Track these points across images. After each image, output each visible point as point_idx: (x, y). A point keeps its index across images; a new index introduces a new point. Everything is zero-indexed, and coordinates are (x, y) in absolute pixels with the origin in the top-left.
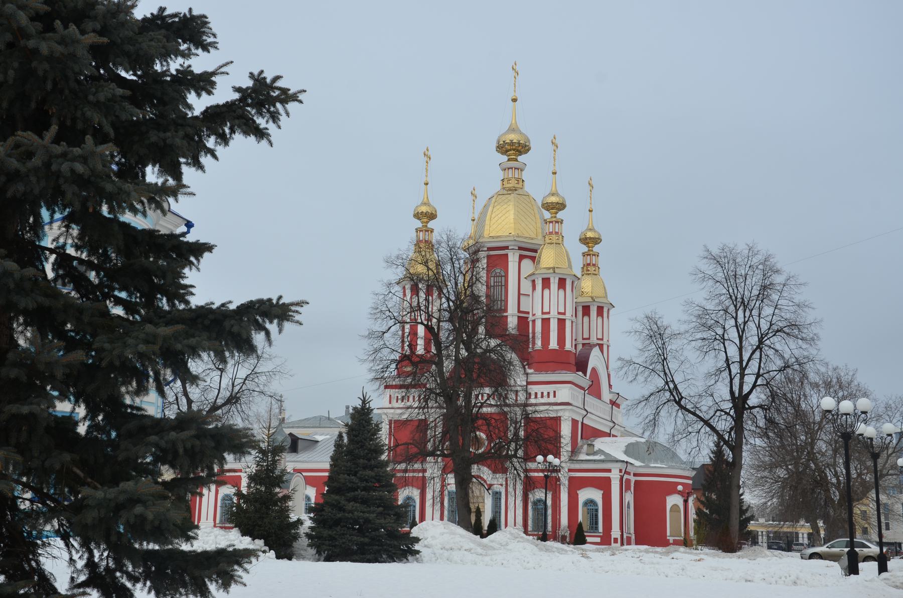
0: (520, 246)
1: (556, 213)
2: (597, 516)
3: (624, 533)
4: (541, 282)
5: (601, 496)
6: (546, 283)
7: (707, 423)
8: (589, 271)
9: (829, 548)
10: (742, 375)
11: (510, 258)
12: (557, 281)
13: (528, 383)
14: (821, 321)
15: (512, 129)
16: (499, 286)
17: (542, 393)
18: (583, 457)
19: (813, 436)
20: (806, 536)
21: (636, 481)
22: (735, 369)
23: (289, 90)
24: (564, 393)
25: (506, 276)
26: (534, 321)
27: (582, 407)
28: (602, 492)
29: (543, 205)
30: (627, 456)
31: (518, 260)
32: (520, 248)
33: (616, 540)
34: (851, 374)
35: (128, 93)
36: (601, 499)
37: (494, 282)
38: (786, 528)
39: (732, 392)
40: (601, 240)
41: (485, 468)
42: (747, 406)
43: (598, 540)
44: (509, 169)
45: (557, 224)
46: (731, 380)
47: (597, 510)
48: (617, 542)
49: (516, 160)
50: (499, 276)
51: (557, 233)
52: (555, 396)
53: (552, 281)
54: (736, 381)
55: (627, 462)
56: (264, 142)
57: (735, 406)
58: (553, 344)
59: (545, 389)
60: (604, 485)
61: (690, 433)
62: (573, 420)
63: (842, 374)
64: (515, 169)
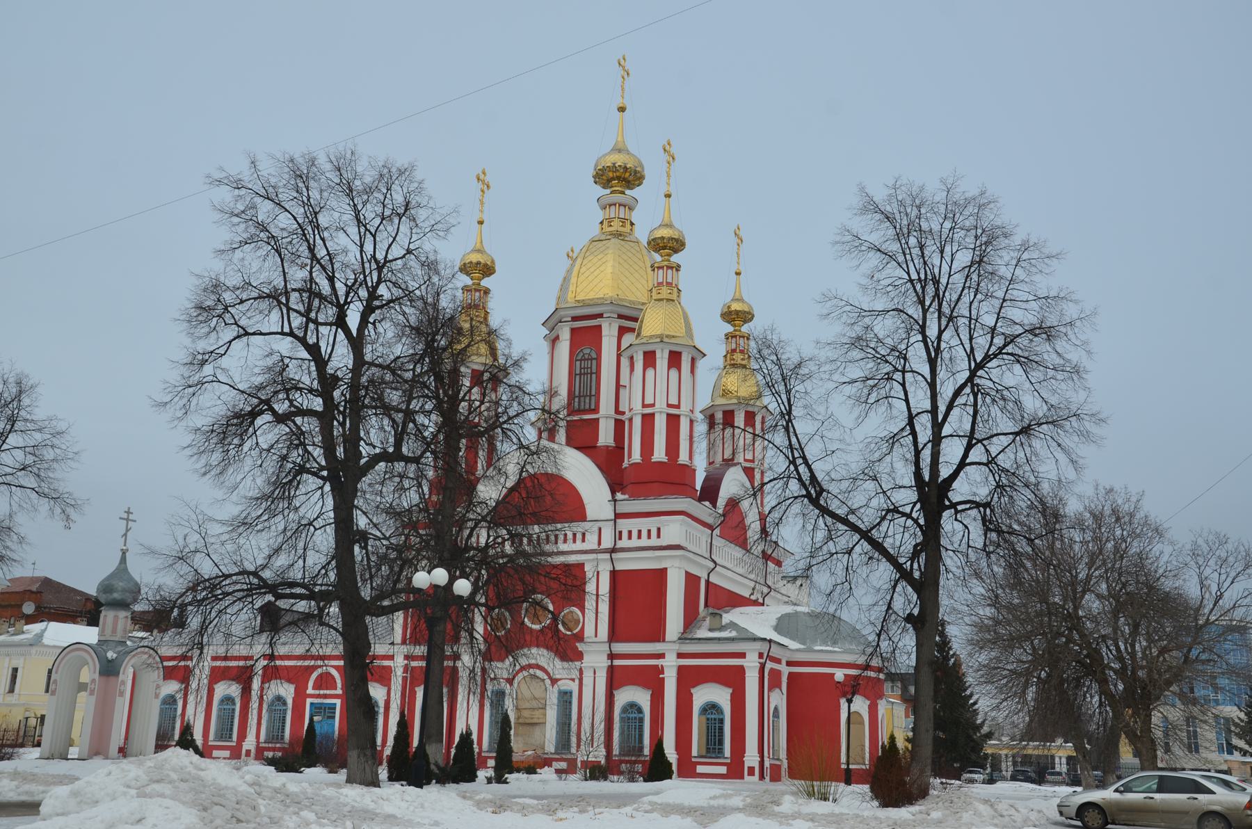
0: (620, 313)
1: (670, 255)
2: (721, 729)
3: (766, 759)
4: (642, 357)
5: (729, 698)
6: (650, 359)
7: (865, 535)
8: (734, 359)
9: (1121, 792)
10: (937, 439)
11: (605, 331)
12: (666, 355)
13: (618, 516)
14: (1094, 313)
15: (618, 150)
16: (584, 368)
17: (640, 532)
18: (703, 633)
19: (1076, 591)
20: (1064, 761)
21: (790, 674)
22: (925, 434)
24: (674, 531)
25: (599, 359)
26: (631, 420)
27: (707, 555)
28: (730, 691)
29: (649, 243)
30: (779, 633)
31: (616, 334)
32: (620, 317)
33: (751, 771)
34: (1134, 499)
36: (649, 703)
37: (581, 368)
38: (1033, 748)
39: (918, 474)
40: (753, 316)
41: (534, 650)
42: (947, 503)
43: (723, 770)
44: (610, 205)
45: (670, 271)
46: (917, 453)
47: (722, 721)
48: (754, 775)
49: (623, 193)
50: (588, 359)
51: (669, 284)
52: (659, 536)
53: (658, 355)
54: (926, 455)
55: (770, 641)
57: (923, 499)
58: (659, 454)
59: (644, 524)
60: (733, 678)
61: (832, 555)
62: (688, 574)
63: (1120, 502)
64: (620, 205)
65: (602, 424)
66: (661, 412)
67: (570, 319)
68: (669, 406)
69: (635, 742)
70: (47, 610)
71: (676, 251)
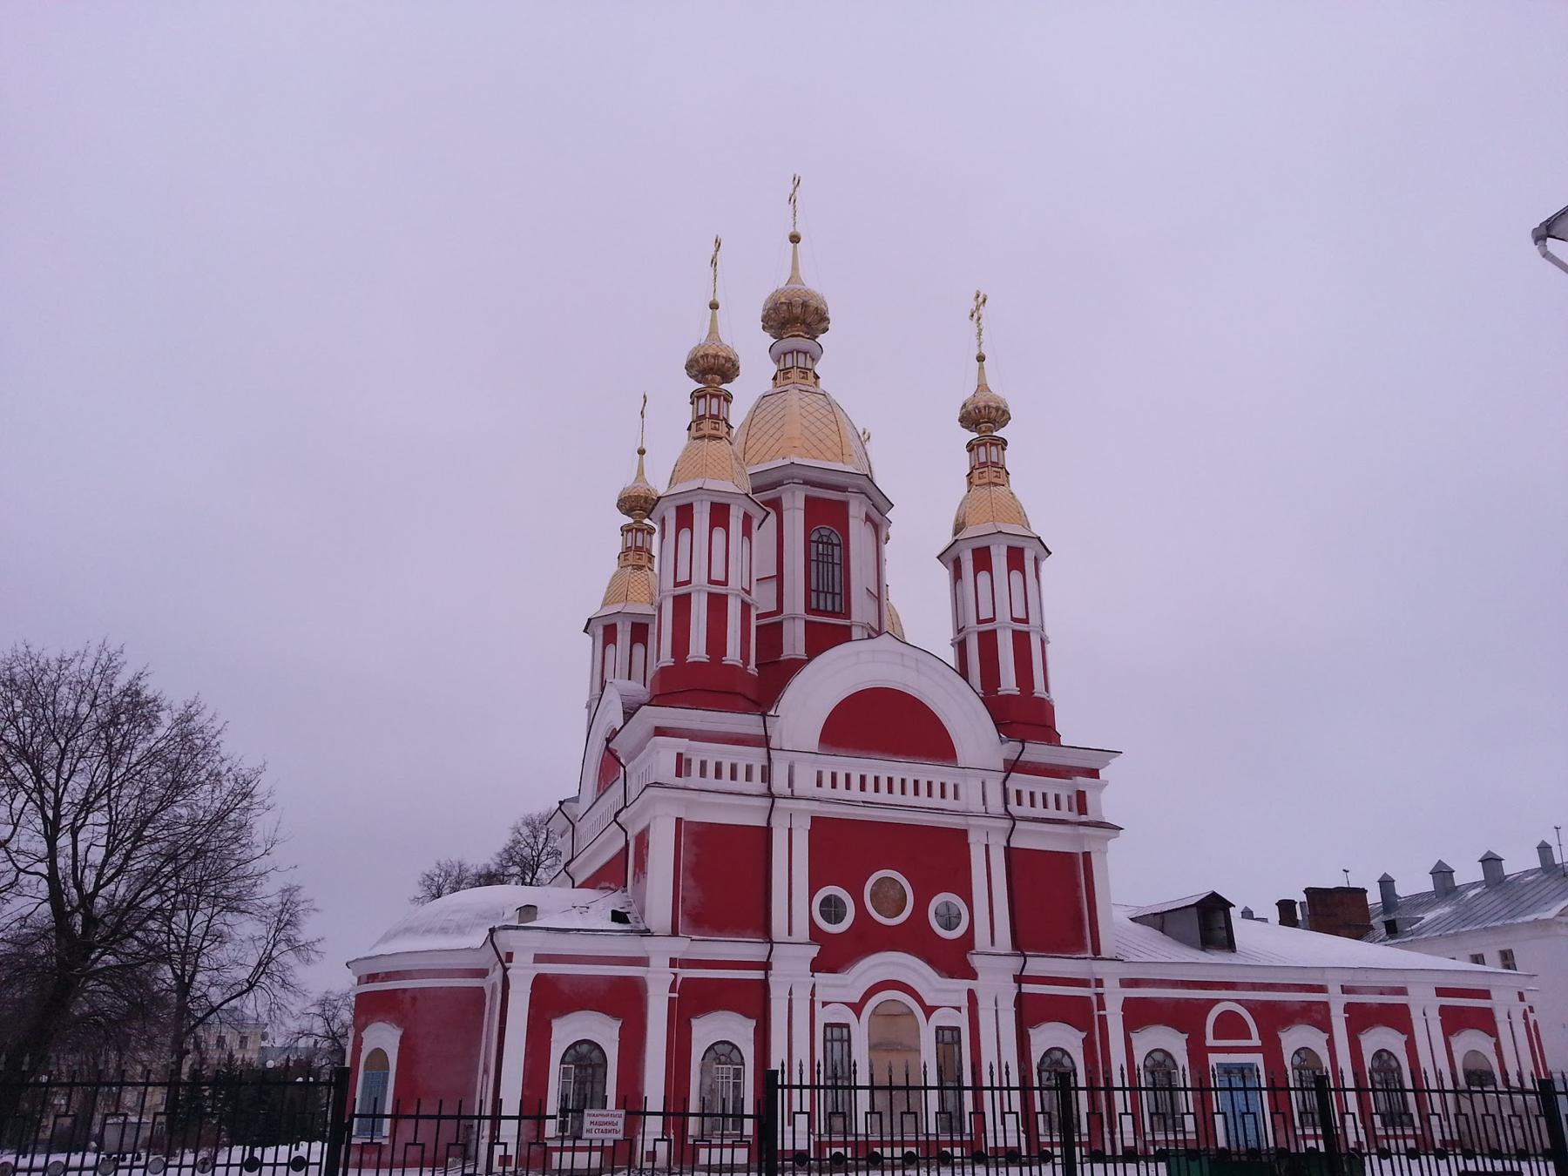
13: (1013, 767)
28: (619, 1024)
32: (806, 483)
36: (396, 1051)
45: (639, 534)
51: (995, 464)
52: (956, 797)
58: (698, 649)
60: (1398, 1018)
64: (798, 352)
65: (800, 608)
68: (1014, 620)
69: (1399, 1106)
70: (125, 904)
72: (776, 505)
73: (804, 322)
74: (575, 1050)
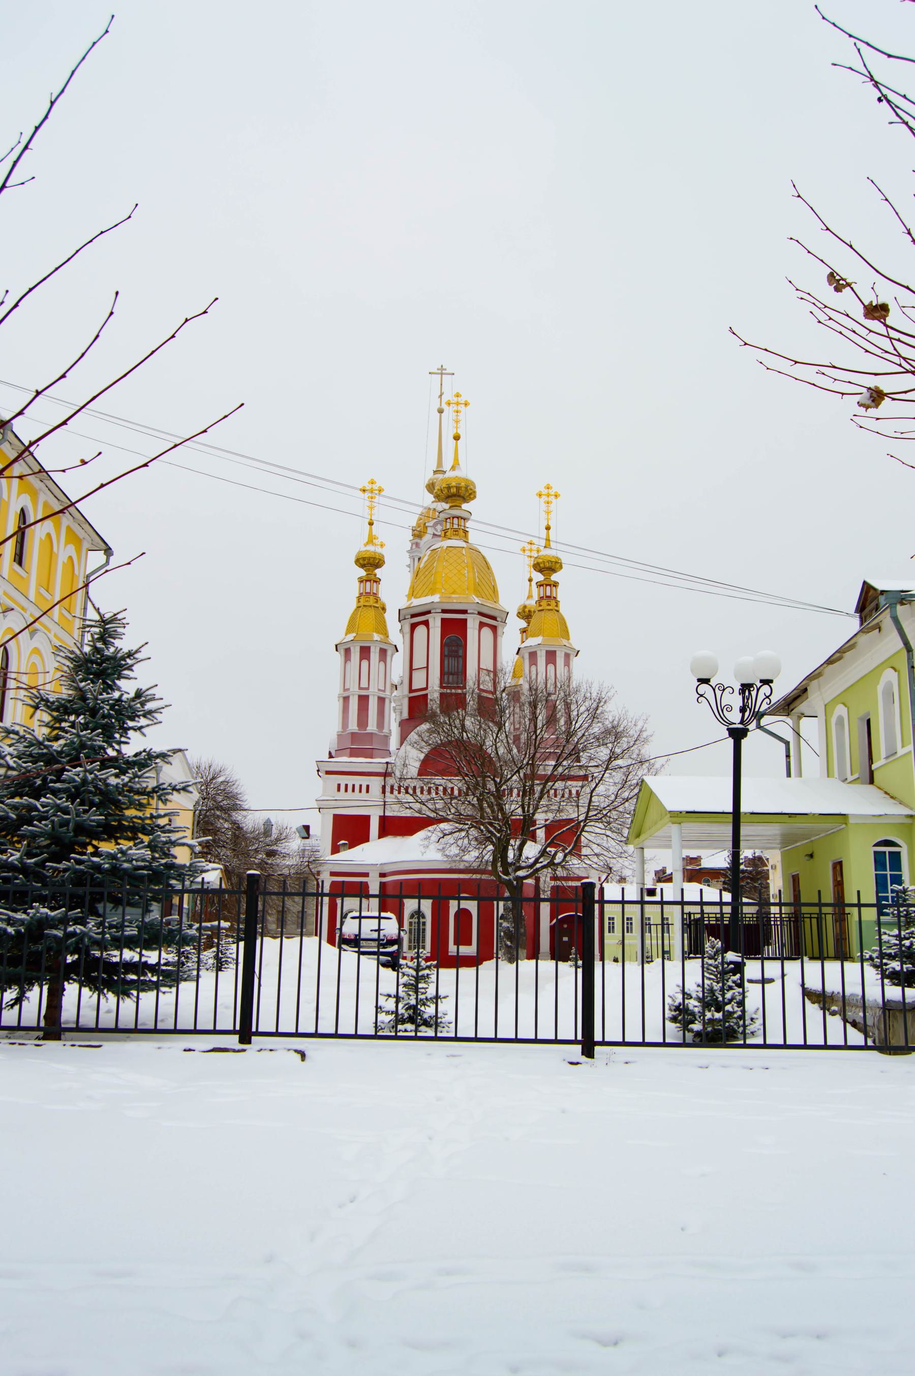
23: (872, 302)
32: (480, 614)
35: (827, 1011)
56: (650, 739)
65: (437, 688)
66: (374, 695)
67: (440, 611)
71: (554, 571)
72: (426, 623)
73: (459, 496)
74: (902, 916)
